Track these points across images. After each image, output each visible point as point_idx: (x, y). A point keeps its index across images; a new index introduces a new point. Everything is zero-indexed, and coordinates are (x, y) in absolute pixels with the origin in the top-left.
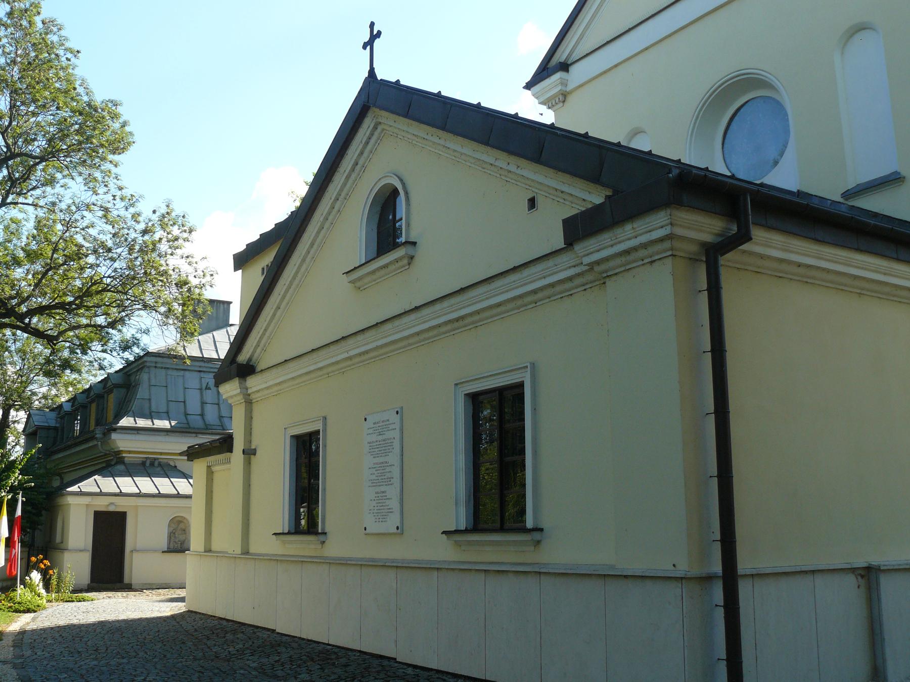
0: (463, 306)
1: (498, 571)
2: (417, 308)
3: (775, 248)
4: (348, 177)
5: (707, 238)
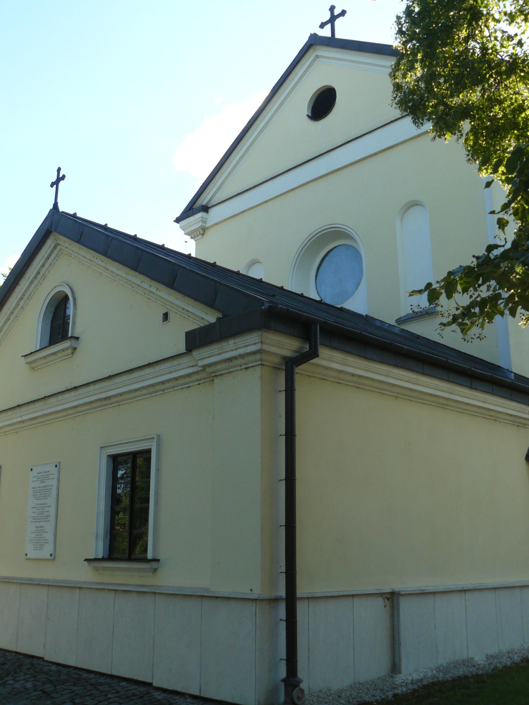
0: (110, 389)
1: (125, 591)
2: (76, 388)
3: (337, 363)
4: (31, 283)
5: (288, 353)
